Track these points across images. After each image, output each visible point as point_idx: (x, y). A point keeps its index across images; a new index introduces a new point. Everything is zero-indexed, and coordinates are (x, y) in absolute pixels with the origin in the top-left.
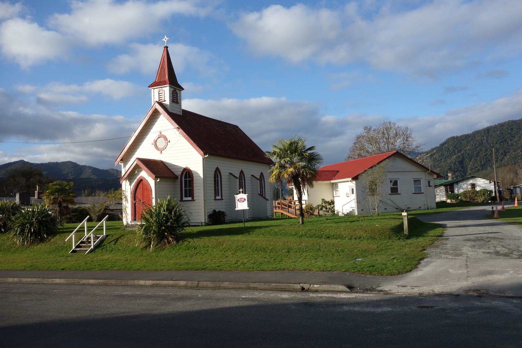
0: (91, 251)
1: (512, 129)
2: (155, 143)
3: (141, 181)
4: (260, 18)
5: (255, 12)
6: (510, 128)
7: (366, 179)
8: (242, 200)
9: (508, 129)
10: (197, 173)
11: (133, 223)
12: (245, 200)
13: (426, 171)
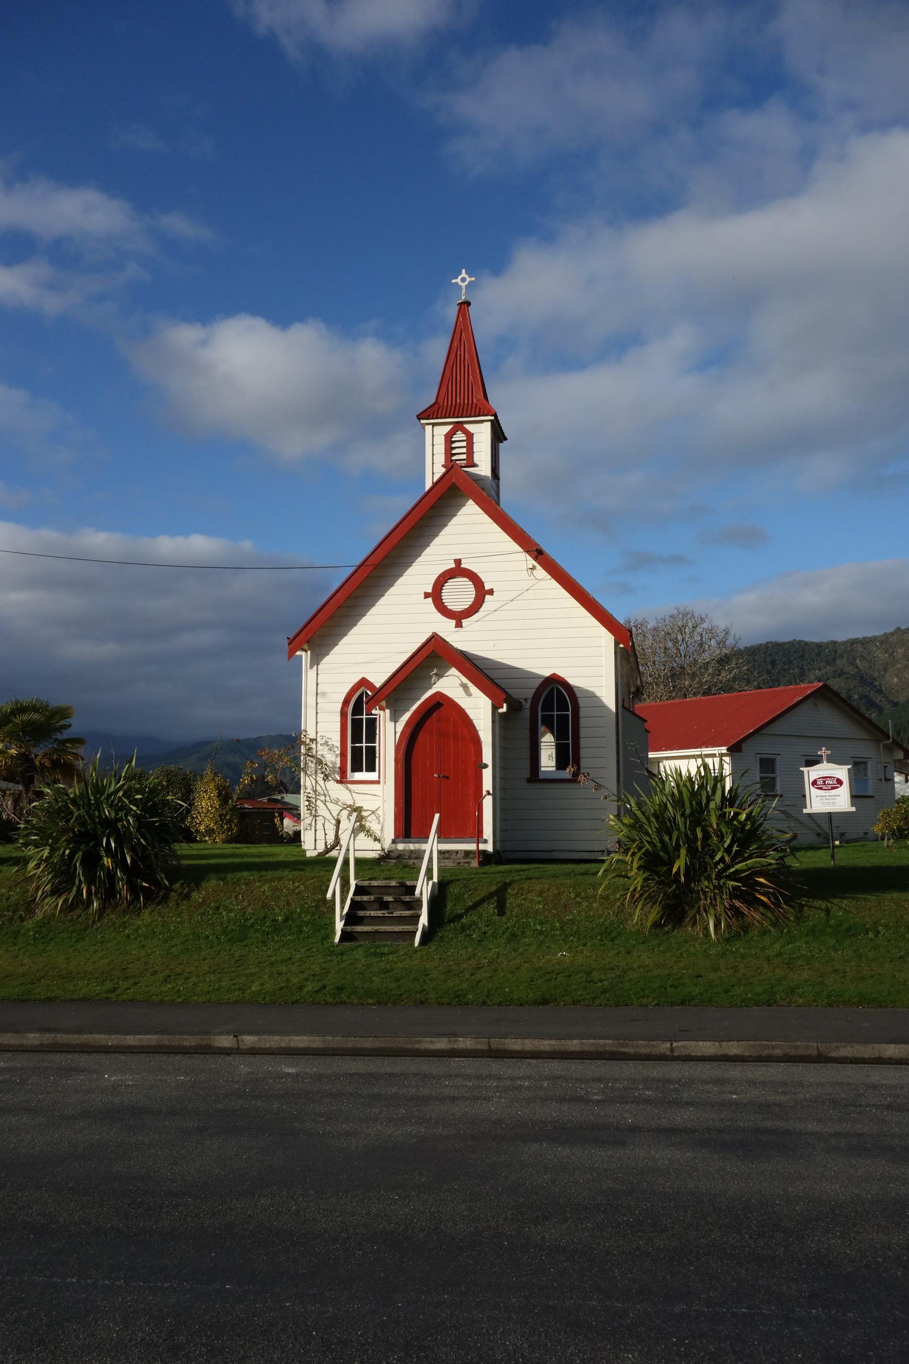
0: (427, 936)
1: (773, 662)
2: (435, 595)
3: (440, 703)
4: (204, 343)
5: (198, 325)
6: (769, 660)
7: (754, 750)
8: (829, 784)
9: (765, 661)
10: (592, 696)
11: (401, 847)
12: (840, 782)
13: (878, 741)
